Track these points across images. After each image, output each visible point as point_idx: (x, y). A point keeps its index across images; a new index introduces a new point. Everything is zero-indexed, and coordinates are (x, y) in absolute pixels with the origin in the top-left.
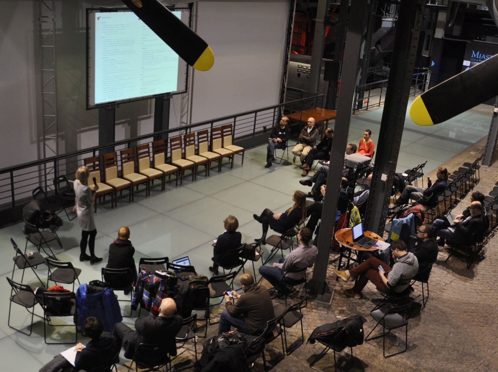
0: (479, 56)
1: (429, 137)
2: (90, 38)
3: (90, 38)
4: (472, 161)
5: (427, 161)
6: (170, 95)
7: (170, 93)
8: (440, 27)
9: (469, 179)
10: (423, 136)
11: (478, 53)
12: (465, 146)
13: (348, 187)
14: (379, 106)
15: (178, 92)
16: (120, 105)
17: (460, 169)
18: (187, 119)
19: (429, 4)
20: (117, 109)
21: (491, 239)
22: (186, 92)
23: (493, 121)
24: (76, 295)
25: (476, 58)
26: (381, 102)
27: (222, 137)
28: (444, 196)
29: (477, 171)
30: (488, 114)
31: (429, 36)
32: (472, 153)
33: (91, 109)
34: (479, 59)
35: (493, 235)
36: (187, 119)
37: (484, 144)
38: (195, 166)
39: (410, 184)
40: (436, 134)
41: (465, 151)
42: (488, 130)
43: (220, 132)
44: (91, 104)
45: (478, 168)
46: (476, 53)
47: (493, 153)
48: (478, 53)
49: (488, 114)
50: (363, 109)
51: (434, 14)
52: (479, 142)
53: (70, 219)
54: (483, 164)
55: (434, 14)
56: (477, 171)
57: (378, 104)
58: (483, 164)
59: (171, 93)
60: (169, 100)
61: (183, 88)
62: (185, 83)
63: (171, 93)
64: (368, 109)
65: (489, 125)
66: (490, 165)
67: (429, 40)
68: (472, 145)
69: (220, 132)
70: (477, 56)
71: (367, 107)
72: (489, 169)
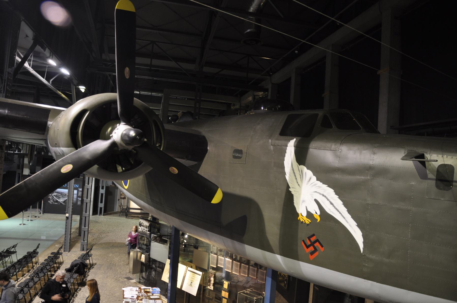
1: (25, 241)
4: (56, 251)
5: (39, 244)
8: (26, 168)
9: (56, 263)
10: (21, 241)
12: (51, 243)
13: (136, 76)
17: (49, 257)
19: (17, 152)
21: (76, 298)
23: (66, 223)
28: (29, 287)
29: (61, 256)
30: (62, 220)
31: (19, 174)
32: (56, 246)
35: (76, 296)
37: (63, 239)
40: (30, 238)
41: (52, 245)
42: (64, 230)
45: (61, 254)
47: (70, 243)
49: (62, 220)
51: (21, 160)
52: (61, 238)
54: (64, 251)
55: (21, 160)
56: (61, 256)
58: (64, 251)
65: (64, 226)
66: (69, 251)
67: (19, 177)
68: (56, 241)
72: (69, 254)
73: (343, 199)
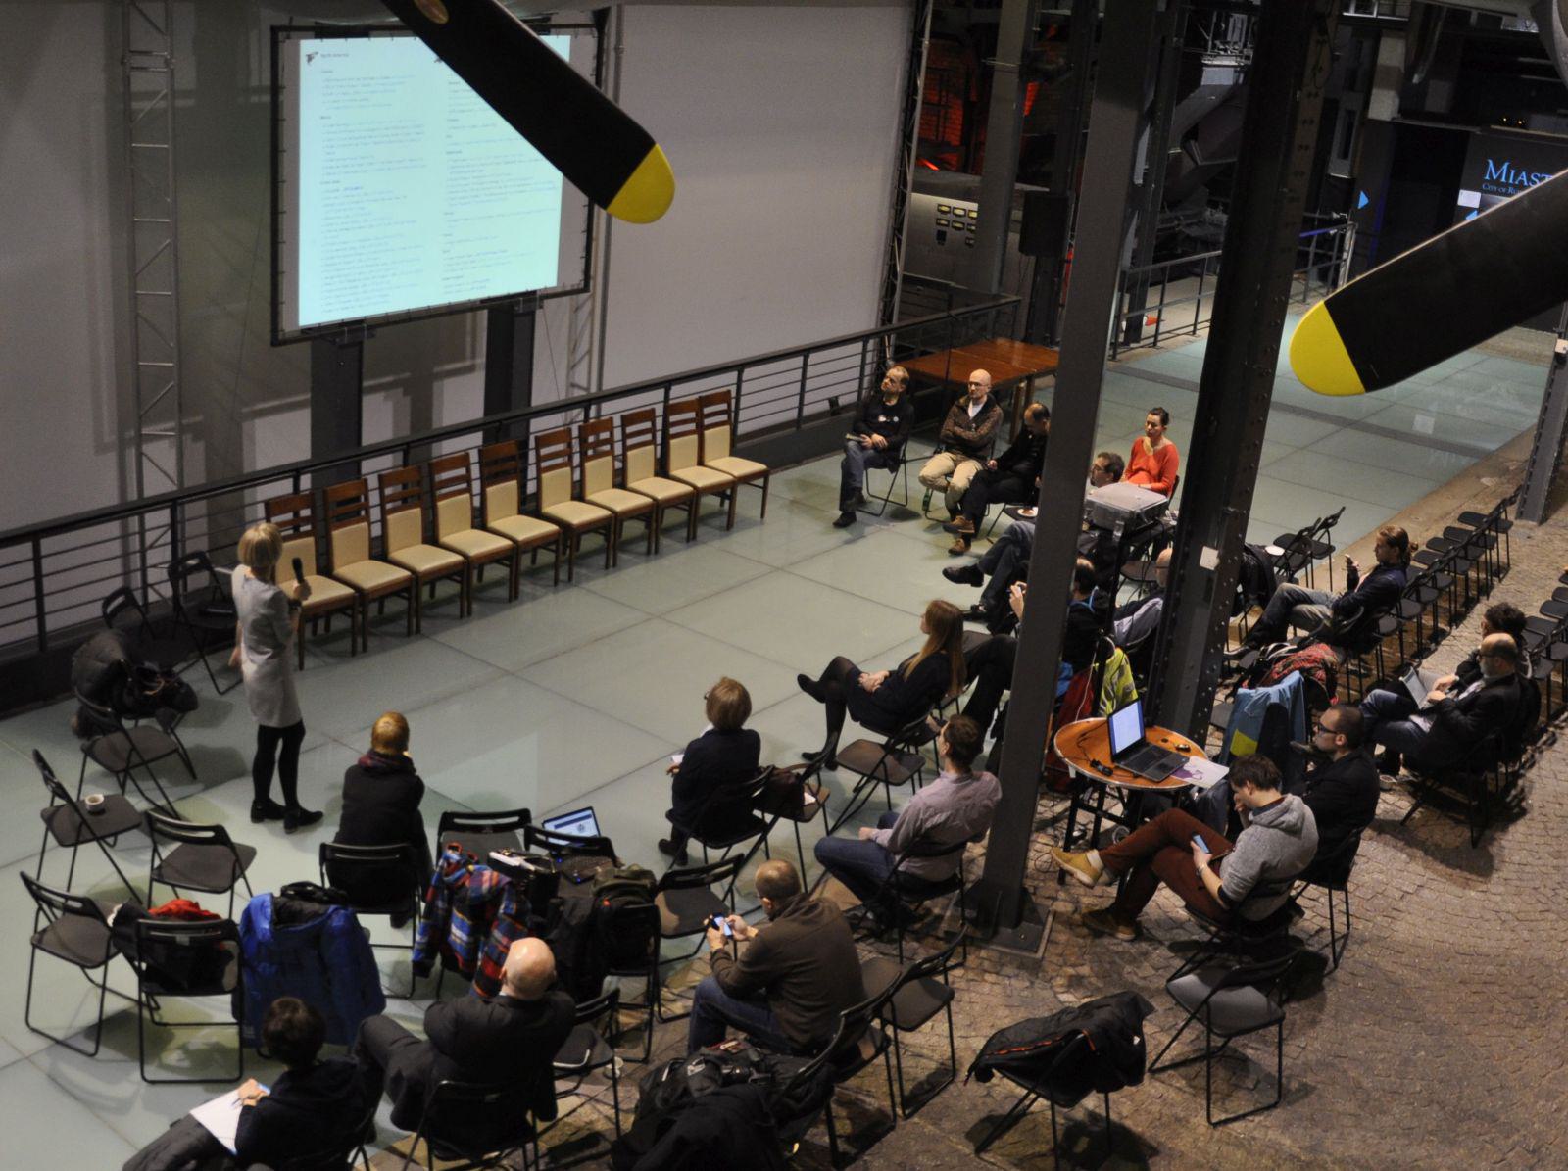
0: (1508, 178)
1: (1350, 432)
2: (284, 120)
3: (284, 120)
4: (1485, 508)
5: (1343, 508)
6: (535, 299)
7: (534, 293)
8: (1386, 86)
9: (1476, 564)
10: (1331, 427)
11: (1505, 167)
12: (1465, 461)
14: (1194, 332)
15: (559, 290)
16: (379, 331)
17: (1448, 531)
18: (589, 373)
19: (1352, 13)
20: (367, 344)
21: (1547, 754)
22: (586, 289)
23: (1551, 382)
24: (239, 928)
25: (1497, 182)
26: (1199, 321)
27: (700, 430)
28: (1399, 616)
29: (1502, 537)
30: (1536, 358)
31: (1351, 113)
32: (1485, 481)
33: (285, 342)
34: (1507, 185)
35: (1553, 741)
36: (589, 373)
37: (1523, 453)
38: (613, 522)
39: (1291, 580)
40: (1374, 421)
41: (1463, 475)
42: (1537, 410)
43: (692, 415)
44: (287, 327)
45: (1505, 528)
46: (1497, 168)
47: (1553, 481)
48: (1505, 167)
49: (1536, 358)
50: (1142, 343)
51: (1367, 45)
52: (1508, 446)
53: (222, 689)
54: (1520, 515)
55: (1367, 45)
56: (1502, 537)
57: (1191, 328)
58: (1520, 515)
59: (539, 293)
60: (532, 314)
61: (576, 279)
62: (584, 260)
63: (539, 293)
64: (1159, 344)
65: (1541, 393)
66: (1543, 520)
67: (1350, 127)
68: (1486, 455)
69: (692, 415)
70: (1500, 177)
71: (1156, 336)
72: (1539, 533)
73: (1408, 699)
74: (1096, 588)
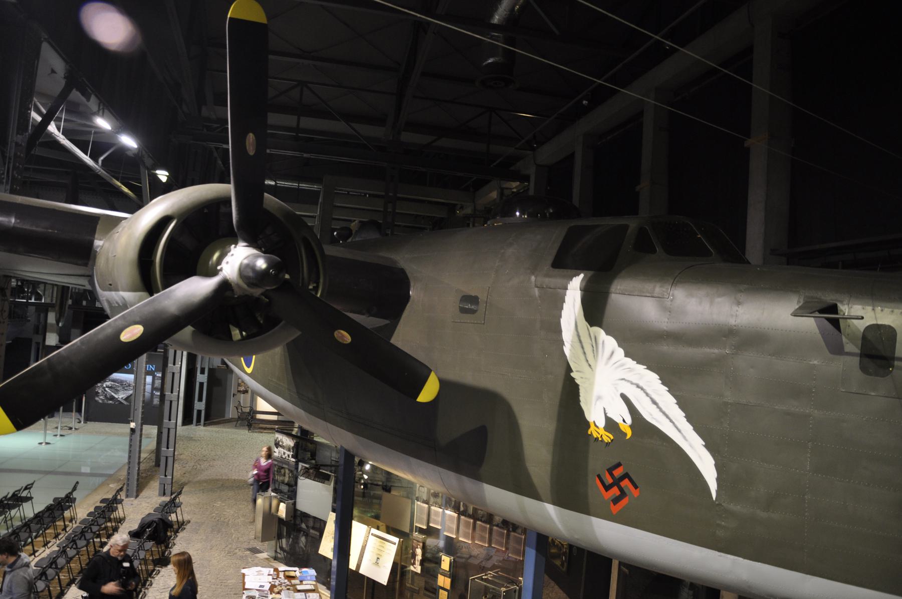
1: (50, 477)
4: (110, 496)
5: (77, 483)
8: (52, 331)
9: (110, 520)
10: (41, 476)
12: (101, 480)
17: (96, 508)
19: (33, 301)
21: (151, 589)
23: (131, 440)
28: (56, 568)
29: (119, 506)
30: (121, 435)
31: (38, 344)
32: (111, 486)
35: (151, 585)
37: (124, 473)
40: (60, 470)
41: (102, 485)
42: (127, 455)
45: (121, 502)
47: (138, 480)
49: (121, 435)
51: (42, 315)
52: (120, 470)
54: (127, 496)
55: (42, 315)
56: (119, 506)
58: (127, 496)
65: (127, 447)
66: (137, 496)
67: (38, 349)
68: (111, 476)
72: (136, 502)
74: (268, 151)
